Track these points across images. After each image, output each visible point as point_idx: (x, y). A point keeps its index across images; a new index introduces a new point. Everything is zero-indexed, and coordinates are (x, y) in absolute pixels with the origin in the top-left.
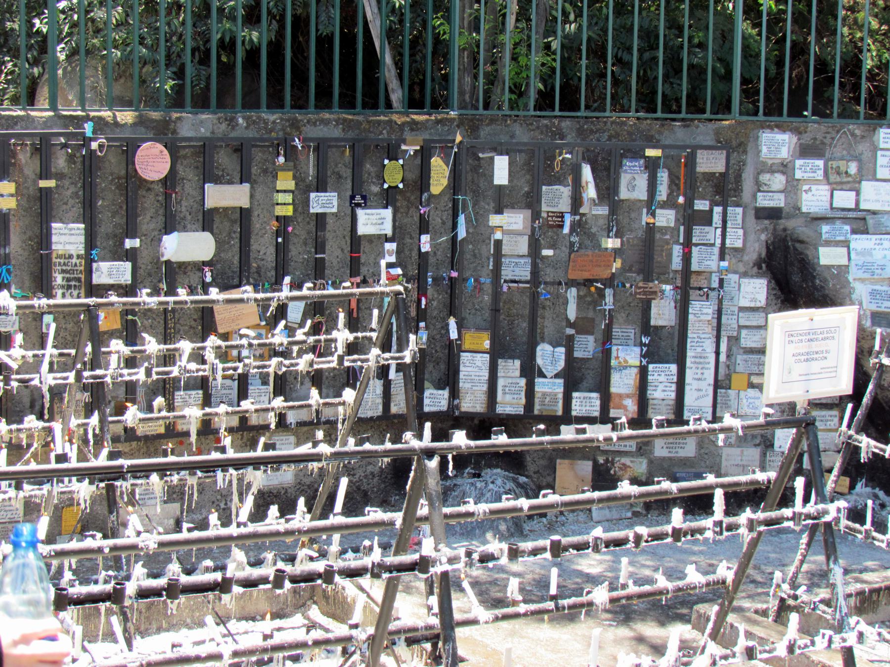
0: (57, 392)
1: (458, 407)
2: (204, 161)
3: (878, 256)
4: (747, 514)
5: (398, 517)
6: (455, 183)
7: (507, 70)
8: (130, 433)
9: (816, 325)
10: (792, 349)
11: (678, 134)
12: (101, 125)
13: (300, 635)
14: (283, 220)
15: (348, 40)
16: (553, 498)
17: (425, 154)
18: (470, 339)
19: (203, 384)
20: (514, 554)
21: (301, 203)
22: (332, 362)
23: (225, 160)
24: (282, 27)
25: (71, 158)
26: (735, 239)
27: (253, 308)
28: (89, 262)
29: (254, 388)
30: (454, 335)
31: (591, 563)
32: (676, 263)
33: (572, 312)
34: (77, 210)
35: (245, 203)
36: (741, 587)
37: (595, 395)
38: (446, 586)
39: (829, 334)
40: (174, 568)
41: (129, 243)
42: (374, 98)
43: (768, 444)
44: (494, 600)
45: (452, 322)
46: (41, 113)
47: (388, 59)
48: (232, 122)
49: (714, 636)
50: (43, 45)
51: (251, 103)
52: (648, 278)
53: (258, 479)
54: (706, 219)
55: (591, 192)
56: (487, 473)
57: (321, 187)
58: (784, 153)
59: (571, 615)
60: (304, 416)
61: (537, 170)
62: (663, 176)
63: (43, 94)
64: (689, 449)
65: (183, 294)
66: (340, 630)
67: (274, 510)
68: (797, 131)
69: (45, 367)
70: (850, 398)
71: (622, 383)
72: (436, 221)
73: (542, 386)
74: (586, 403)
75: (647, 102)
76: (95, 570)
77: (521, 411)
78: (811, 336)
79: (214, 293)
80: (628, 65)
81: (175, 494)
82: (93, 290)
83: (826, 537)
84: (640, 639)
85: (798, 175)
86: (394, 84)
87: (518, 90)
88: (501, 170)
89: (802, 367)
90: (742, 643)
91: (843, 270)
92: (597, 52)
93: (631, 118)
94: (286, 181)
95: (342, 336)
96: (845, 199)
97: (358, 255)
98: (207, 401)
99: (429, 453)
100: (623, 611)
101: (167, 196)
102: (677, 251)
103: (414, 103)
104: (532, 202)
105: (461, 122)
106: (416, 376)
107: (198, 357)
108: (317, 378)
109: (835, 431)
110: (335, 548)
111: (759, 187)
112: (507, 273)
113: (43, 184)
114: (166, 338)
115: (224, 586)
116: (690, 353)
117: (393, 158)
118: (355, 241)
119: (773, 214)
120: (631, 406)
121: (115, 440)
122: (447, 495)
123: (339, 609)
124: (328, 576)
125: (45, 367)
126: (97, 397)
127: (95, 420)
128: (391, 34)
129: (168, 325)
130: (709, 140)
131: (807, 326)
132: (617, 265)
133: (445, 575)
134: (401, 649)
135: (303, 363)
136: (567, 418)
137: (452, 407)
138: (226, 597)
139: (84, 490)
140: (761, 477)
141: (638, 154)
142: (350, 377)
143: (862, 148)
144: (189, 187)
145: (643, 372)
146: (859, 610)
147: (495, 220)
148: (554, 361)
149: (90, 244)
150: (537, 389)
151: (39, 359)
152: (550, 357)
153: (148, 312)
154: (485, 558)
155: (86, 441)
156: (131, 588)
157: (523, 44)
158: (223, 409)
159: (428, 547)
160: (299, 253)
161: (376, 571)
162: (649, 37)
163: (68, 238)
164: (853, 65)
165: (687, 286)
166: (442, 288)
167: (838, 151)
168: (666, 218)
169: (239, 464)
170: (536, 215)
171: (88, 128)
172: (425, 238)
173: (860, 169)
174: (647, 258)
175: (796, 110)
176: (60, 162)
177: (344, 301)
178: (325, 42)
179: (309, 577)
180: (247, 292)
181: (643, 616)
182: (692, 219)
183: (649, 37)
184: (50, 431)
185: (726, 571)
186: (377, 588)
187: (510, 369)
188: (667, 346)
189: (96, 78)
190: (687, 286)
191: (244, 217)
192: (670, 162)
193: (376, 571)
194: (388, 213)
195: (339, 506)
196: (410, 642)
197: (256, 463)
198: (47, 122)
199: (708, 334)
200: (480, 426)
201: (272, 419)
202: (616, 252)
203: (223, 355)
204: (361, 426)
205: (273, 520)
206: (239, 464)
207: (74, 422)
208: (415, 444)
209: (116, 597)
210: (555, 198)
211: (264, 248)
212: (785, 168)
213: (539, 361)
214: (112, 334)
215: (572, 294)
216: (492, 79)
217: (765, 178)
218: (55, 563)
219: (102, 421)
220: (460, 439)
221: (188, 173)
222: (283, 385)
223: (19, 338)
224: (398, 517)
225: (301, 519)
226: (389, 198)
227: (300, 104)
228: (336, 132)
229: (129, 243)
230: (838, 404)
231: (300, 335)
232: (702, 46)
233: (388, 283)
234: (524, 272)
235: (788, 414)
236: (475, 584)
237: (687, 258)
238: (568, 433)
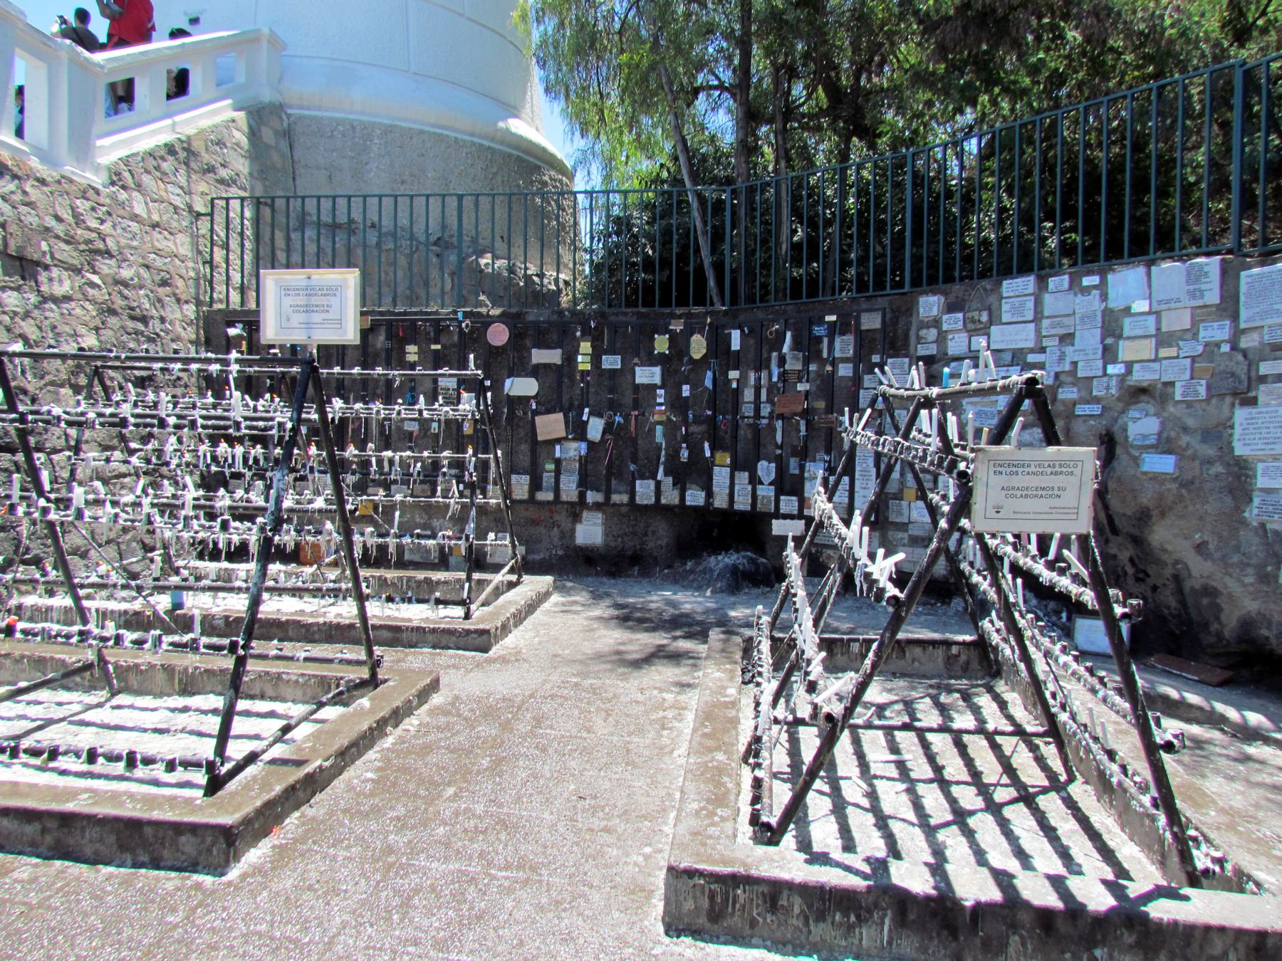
1: (712, 504)
9: (313, 283)
10: (288, 301)
18: (718, 455)
30: (708, 454)
37: (794, 498)
58: (935, 312)
68: (945, 293)
77: (749, 508)
85: (945, 327)
94: (586, 347)
111: (919, 340)
116: (858, 468)
131: (304, 283)
143: (992, 299)
148: (768, 474)
150: (759, 493)
152: (766, 470)
167: (975, 304)
173: (990, 315)
187: (743, 477)
212: (936, 323)
213: (760, 473)
217: (923, 333)
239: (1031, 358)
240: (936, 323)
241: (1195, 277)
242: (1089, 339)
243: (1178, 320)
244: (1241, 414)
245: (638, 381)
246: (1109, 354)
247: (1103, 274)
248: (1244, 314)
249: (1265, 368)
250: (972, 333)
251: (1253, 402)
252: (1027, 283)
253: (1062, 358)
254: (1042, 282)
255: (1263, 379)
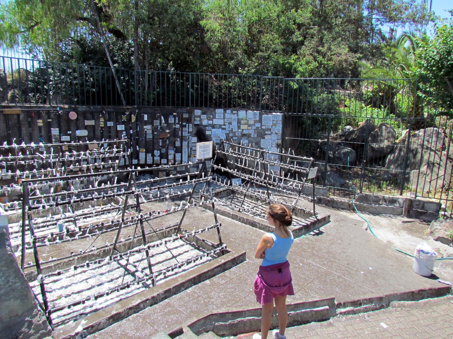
0: (54, 163)
2: (84, 116)
3: (217, 132)
4: (194, 180)
5: (128, 184)
6: (137, 120)
7: (146, 98)
8: (71, 171)
11: (180, 110)
12: (61, 108)
13: (109, 208)
14: (102, 128)
15: (114, 92)
16: (157, 179)
17: (130, 114)
18: (141, 150)
19: (86, 160)
20: (151, 190)
21: (105, 124)
22: (113, 155)
23: (89, 115)
24: (99, 89)
25: (55, 115)
26: (191, 130)
27: (97, 145)
28: (60, 136)
29: (98, 161)
30: (138, 149)
31: (166, 191)
32: (180, 135)
33: (161, 144)
34: (56, 125)
35: (94, 124)
36: (16, 121)
38: (138, 196)
39: (208, 146)
40: (83, 197)
41: (69, 132)
42: (120, 103)
43: (198, 167)
44: (147, 197)
45: (137, 147)
46: (47, 105)
47: (122, 96)
48: (90, 108)
49: (189, 202)
50: (47, 91)
51: (94, 104)
52: (175, 137)
53: (99, 178)
54: (185, 126)
55: (163, 122)
56: (146, 175)
57: (109, 121)
58: (199, 114)
59: (162, 200)
60: (108, 166)
61: (152, 118)
62: (177, 118)
63: (48, 101)
64: (184, 169)
65: (81, 142)
66: (117, 206)
67: (103, 184)
69: (51, 158)
70: (211, 158)
71: (171, 157)
72: (133, 127)
73: (156, 158)
74: (164, 161)
75: (173, 104)
76: (65, 198)
78: (205, 147)
79: (88, 142)
80: (169, 98)
81: (82, 182)
82: (61, 142)
83: (209, 184)
84: (176, 204)
86: (123, 100)
87: (149, 102)
88: (146, 117)
89: (203, 153)
90: (194, 203)
91: (211, 135)
92: (163, 94)
93: (170, 107)
94: (102, 120)
95: (115, 150)
96: (210, 122)
97: (118, 134)
98: (88, 163)
99: (133, 171)
100: (173, 199)
101: (77, 123)
102: (180, 132)
103: (128, 104)
104: (152, 124)
105: (137, 108)
106: (131, 157)
107: (85, 155)
108: (111, 158)
109: (210, 164)
110: (115, 191)
111: (195, 120)
112: (148, 137)
113: (49, 120)
114: (78, 151)
115: (92, 199)
117: (124, 115)
118: (117, 131)
119: (197, 125)
120: (173, 161)
121: (68, 172)
122: (137, 179)
123: (117, 202)
124: (114, 196)
125: (51, 158)
126: (64, 164)
127: (63, 168)
128: (122, 90)
129: (78, 148)
130: (185, 111)
132: (169, 135)
133: (137, 194)
134: (130, 209)
135: (107, 156)
136: (161, 164)
137: (138, 163)
138: (93, 202)
139: (62, 182)
140: (196, 173)
141: (172, 114)
142: (117, 158)
143: (213, 113)
144: (81, 121)
145: (175, 155)
146: (215, 196)
147: (145, 127)
149: (60, 133)
151: (50, 156)
152: (157, 153)
153: (74, 146)
154: (145, 191)
155: (61, 173)
156: (72, 201)
157: (149, 93)
158: (91, 165)
159: (134, 189)
160: (106, 134)
161: (123, 194)
162: (173, 92)
163: (55, 131)
164: (211, 97)
165: (182, 139)
166: (136, 140)
168: (178, 126)
169: (95, 175)
170: (153, 126)
171: (58, 109)
172: (131, 131)
174: (174, 133)
175: (201, 106)
176: (52, 116)
177: (115, 143)
178: (109, 91)
179: (110, 196)
180: (95, 142)
181: (177, 200)
182: (182, 126)
183: (173, 92)
184: (53, 171)
185: (191, 190)
186: (124, 198)
187: (149, 155)
188: (179, 150)
189: (59, 98)
190: (182, 139)
191: (93, 127)
192: (178, 115)
193: (123, 194)
194: (123, 126)
195: (115, 182)
196: (132, 208)
197: (99, 175)
198: (49, 108)
199: (186, 147)
200: (143, 166)
201: (102, 167)
202: (169, 133)
203: (90, 154)
204: (120, 167)
205: (103, 186)
206: (95, 175)
207: (59, 169)
208: (130, 170)
209: (69, 203)
210: (157, 123)
211: (98, 133)
212: (199, 117)
214: (66, 151)
215: (161, 141)
216: (143, 100)
218: (56, 197)
219: (65, 169)
220: (139, 168)
221: (81, 118)
222: (104, 160)
223: (45, 152)
224: (128, 184)
225: (109, 185)
226: (123, 123)
227: (104, 104)
228: (112, 110)
229: (69, 132)
230: (209, 159)
231: (106, 150)
232: (184, 94)
233: (124, 139)
234: (151, 137)
235: (200, 161)
236: (144, 196)
237: (182, 134)
238: (160, 167)
239: (223, 127)
240: (199, 117)
241: (255, 114)
242: (235, 124)
243: (251, 122)
244: (262, 140)
245: (118, 129)
246: (239, 128)
247: (237, 111)
248: (263, 122)
249: (266, 132)
250: (209, 120)
251: (264, 138)
252: (221, 111)
253: (229, 127)
254: (225, 111)
255: (266, 134)
